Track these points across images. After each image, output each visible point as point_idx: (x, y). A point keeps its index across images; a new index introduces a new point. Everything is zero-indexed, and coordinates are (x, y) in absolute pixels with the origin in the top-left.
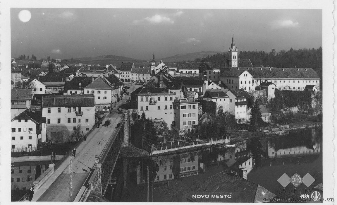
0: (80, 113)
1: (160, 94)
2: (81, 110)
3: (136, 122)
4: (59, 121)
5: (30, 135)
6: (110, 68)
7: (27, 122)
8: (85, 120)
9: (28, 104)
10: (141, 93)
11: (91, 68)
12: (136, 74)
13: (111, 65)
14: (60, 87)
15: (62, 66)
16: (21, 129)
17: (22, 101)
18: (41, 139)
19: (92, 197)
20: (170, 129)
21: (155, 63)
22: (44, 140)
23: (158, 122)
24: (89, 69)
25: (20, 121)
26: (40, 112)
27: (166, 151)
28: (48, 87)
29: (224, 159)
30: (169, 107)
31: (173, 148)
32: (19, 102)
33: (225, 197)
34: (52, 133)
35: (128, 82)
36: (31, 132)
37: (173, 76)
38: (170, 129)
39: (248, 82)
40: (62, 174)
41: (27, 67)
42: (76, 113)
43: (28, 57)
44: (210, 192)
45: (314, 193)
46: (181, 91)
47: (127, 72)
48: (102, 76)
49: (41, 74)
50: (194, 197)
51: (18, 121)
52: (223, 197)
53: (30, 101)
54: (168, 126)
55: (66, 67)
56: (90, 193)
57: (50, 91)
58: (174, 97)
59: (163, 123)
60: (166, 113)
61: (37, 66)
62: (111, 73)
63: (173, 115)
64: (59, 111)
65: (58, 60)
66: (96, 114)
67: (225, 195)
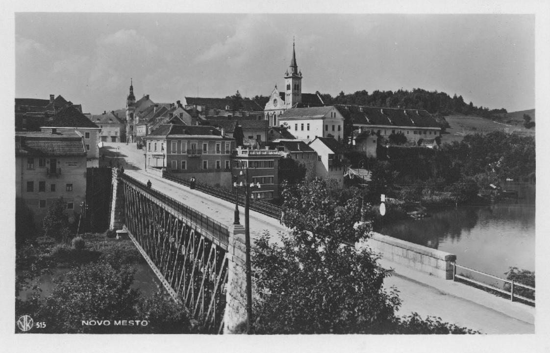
29: (97, 159)
33: (138, 324)
39: (336, 128)
50: (84, 323)
67: (138, 322)
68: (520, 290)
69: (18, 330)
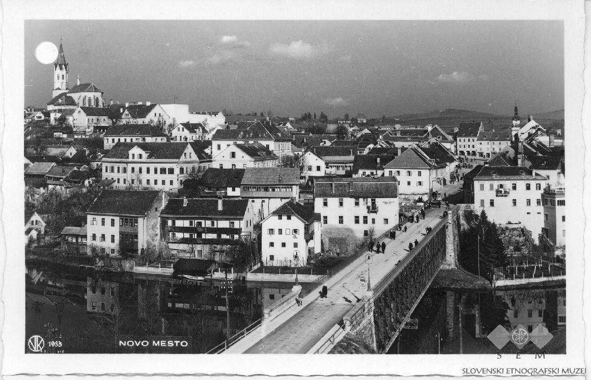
0: (373, 209)
1: (515, 177)
2: (375, 203)
3: (471, 227)
4: (341, 220)
5: (295, 241)
6: (435, 133)
7: (290, 219)
8: (383, 221)
9: (295, 192)
10: (480, 175)
11: (404, 132)
12: (486, 142)
13: (436, 126)
14: (341, 165)
15: (361, 130)
16: (281, 230)
17: (287, 186)
18: (313, 248)
19: (345, 344)
20: (537, 242)
21: (518, 122)
22: (318, 250)
23: (514, 229)
24: (399, 135)
25: (280, 218)
26: (311, 205)
27: (524, 281)
28: (329, 165)
30: (534, 202)
31: (537, 276)
32: (282, 188)
33: (177, 345)
34: (331, 240)
35: (472, 155)
36: (297, 235)
37: (547, 144)
38: (537, 242)
40: (312, 303)
41: (303, 132)
42: (368, 208)
43: (315, 116)
44: (157, 335)
45: (34, 338)
46: (559, 173)
47: (471, 139)
48: (416, 146)
49: (323, 143)
51: (277, 217)
52: (173, 345)
53: (298, 186)
54: (533, 237)
55: (366, 131)
56: (344, 337)
57: (333, 171)
58: (544, 185)
59: (522, 230)
60: (528, 213)
61: (320, 131)
62: (433, 140)
63: (542, 217)
64: (341, 204)
65: (362, 119)
66: (401, 210)
67: (177, 342)
68: (378, 326)
69: (28, 350)
